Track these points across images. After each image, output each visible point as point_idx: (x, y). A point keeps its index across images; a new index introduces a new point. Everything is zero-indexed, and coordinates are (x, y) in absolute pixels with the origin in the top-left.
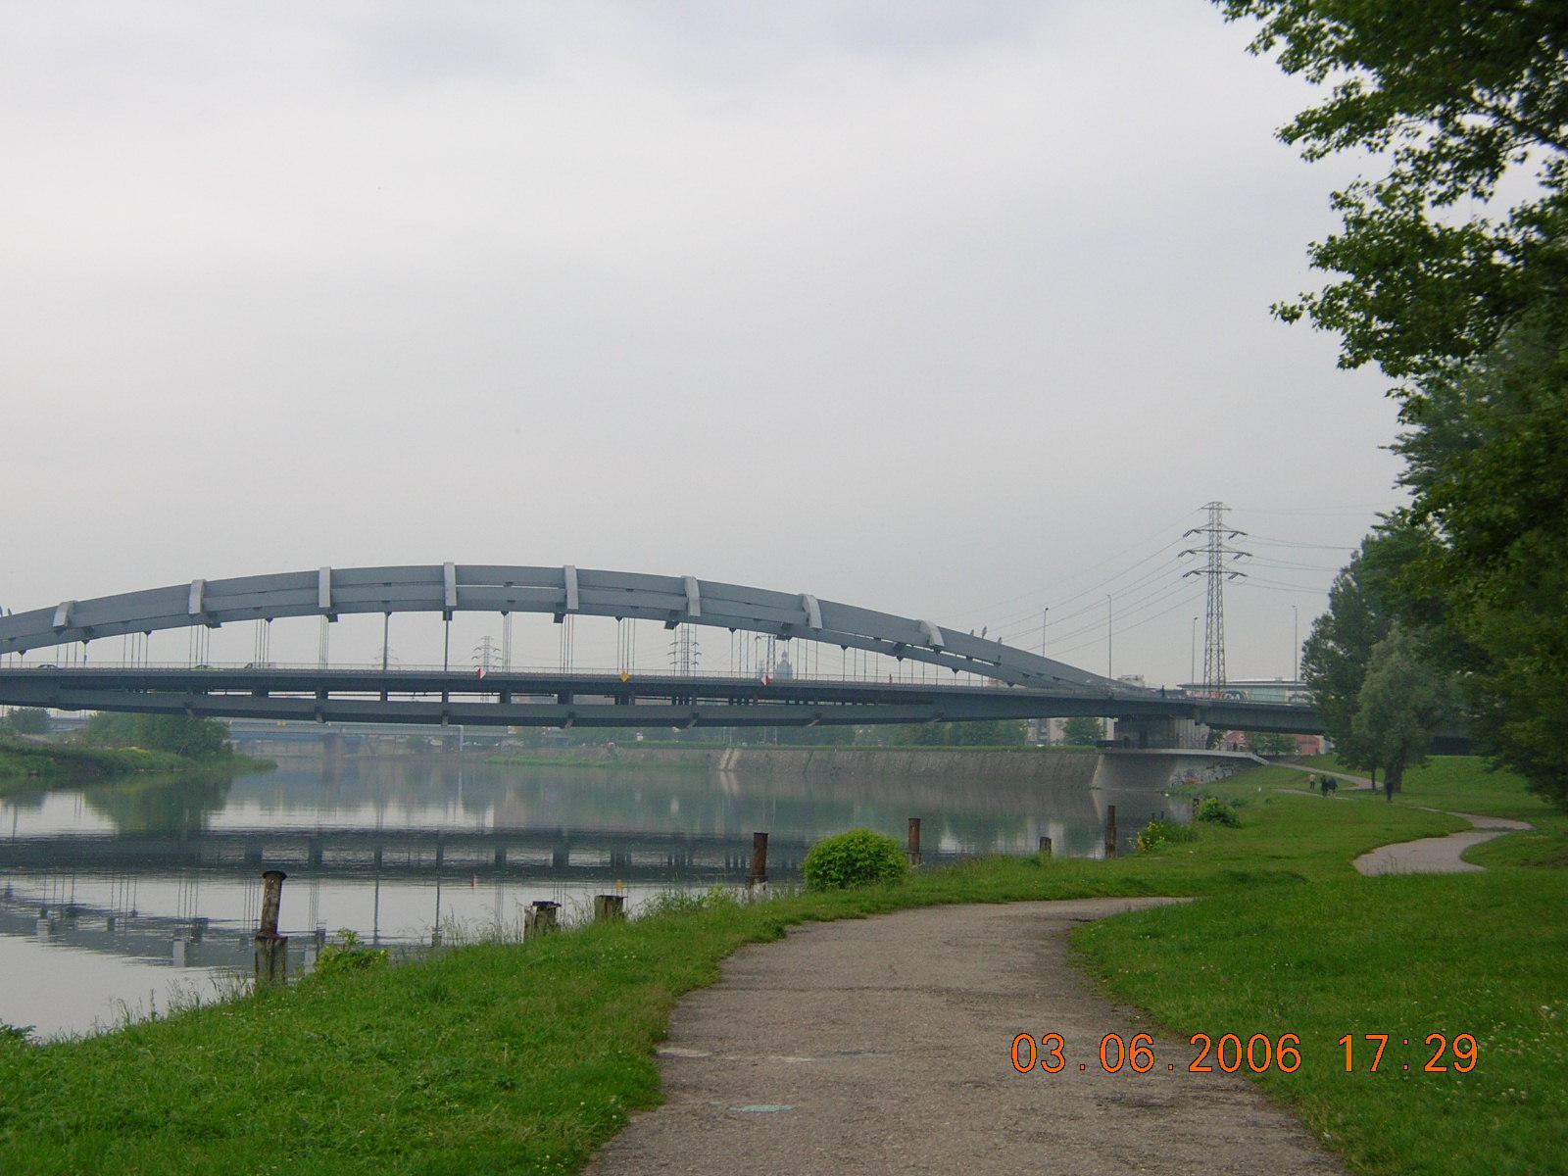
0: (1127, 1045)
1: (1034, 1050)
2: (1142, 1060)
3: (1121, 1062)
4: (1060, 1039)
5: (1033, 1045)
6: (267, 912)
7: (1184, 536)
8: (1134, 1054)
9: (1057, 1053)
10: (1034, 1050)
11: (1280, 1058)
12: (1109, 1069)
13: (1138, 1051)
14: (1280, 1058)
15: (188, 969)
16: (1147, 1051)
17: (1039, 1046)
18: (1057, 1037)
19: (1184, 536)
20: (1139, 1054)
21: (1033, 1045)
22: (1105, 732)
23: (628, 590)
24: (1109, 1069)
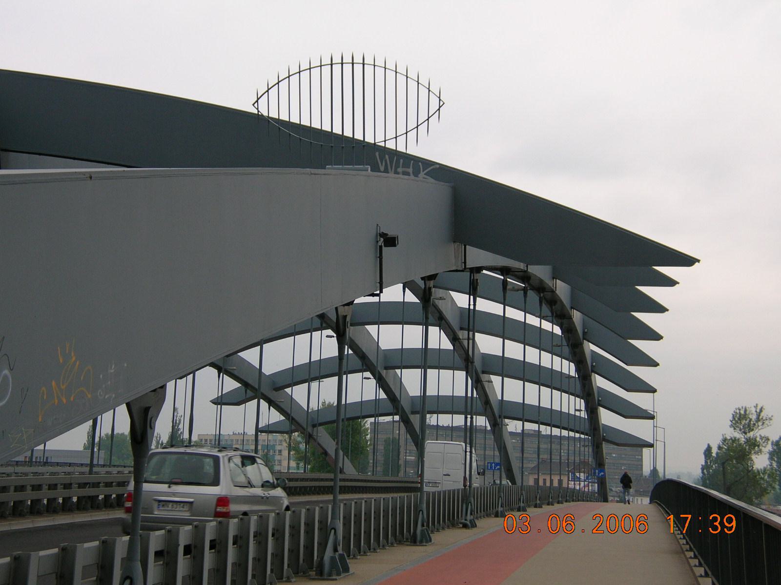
0: (561, 520)
1: (515, 522)
2: (569, 528)
3: (632, 528)
4: (601, 517)
5: (617, 520)
6: (80, 174)
7: (4, 337)
8: (565, 524)
9: (527, 524)
10: (515, 522)
11: (564, 526)
12: (611, 532)
13: (567, 523)
14: (564, 526)
15: (322, 312)
16: (571, 523)
17: (518, 520)
18: (600, 516)
19: (4, 337)
20: (567, 524)
21: (617, 520)
22: (182, 433)
23: (20, 413)
24: (611, 532)
